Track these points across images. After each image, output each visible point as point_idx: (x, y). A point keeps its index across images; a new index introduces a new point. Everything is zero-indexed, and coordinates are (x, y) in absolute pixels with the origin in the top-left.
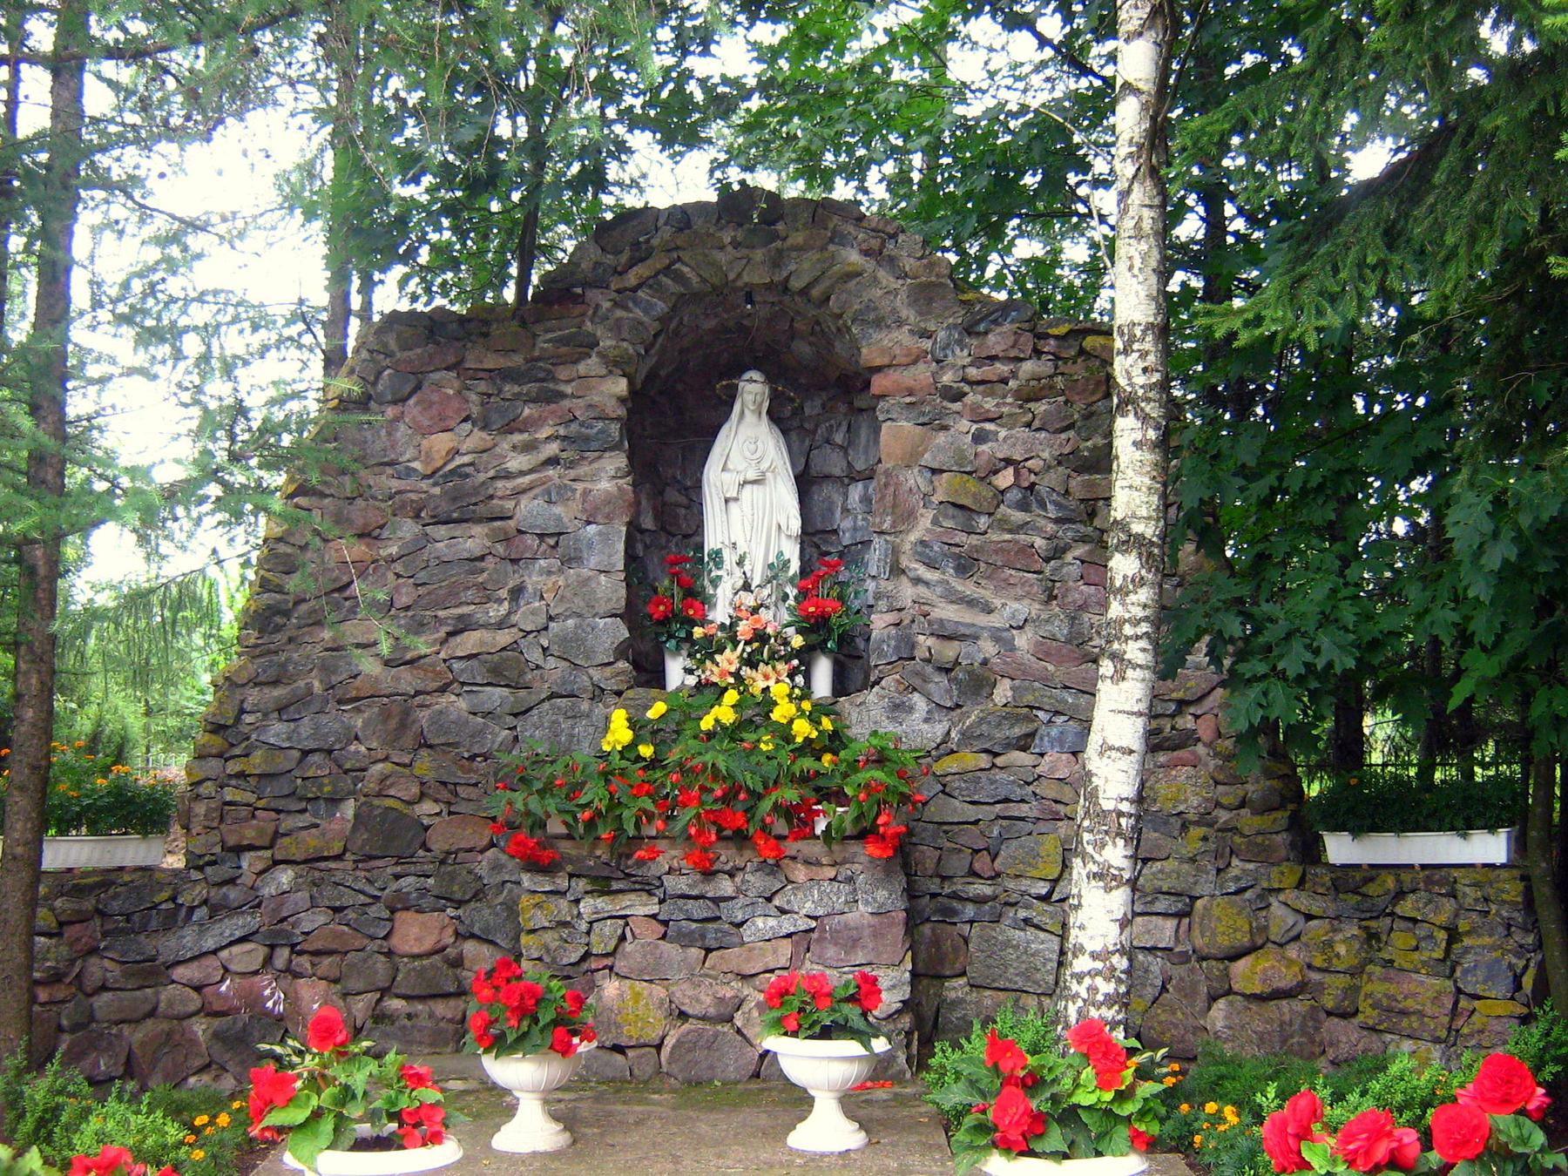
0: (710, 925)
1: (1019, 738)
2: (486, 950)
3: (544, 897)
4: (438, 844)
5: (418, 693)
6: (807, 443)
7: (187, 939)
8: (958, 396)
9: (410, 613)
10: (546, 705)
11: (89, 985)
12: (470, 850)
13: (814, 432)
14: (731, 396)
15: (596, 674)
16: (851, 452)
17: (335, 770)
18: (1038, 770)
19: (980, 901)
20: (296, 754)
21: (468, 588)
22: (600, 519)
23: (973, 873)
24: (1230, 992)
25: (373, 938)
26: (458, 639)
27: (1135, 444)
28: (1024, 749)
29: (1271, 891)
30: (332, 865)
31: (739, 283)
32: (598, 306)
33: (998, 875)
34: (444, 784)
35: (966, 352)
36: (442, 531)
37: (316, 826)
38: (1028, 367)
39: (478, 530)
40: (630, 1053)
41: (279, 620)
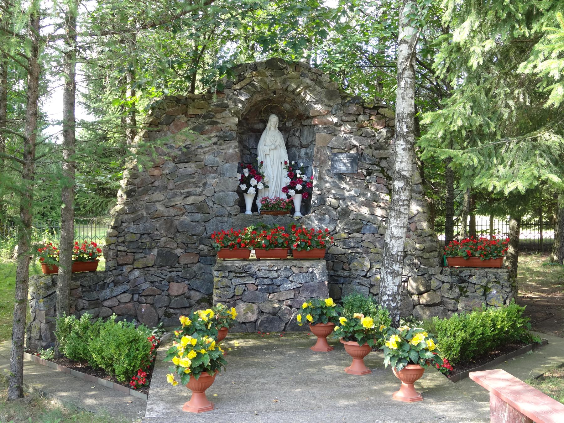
0: (270, 286)
2: (197, 293)
3: (221, 279)
4: (183, 261)
5: (175, 216)
6: (287, 135)
7: (107, 293)
9: (173, 191)
10: (214, 219)
11: (79, 308)
12: (192, 263)
14: (265, 122)
15: (228, 209)
17: (151, 240)
18: (362, 239)
19: (345, 277)
20: (139, 235)
21: (190, 183)
22: (230, 162)
23: (343, 269)
25: (163, 291)
26: (187, 199)
27: (403, 149)
28: (358, 232)
30: (151, 269)
31: (272, 88)
32: (228, 95)
33: (351, 270)
34: (184, 243)
35: (342, 112)
36: (181, 165)
37: (146, 257)
39: (193, 165)
40: (247, 325)
41: (133, 193)
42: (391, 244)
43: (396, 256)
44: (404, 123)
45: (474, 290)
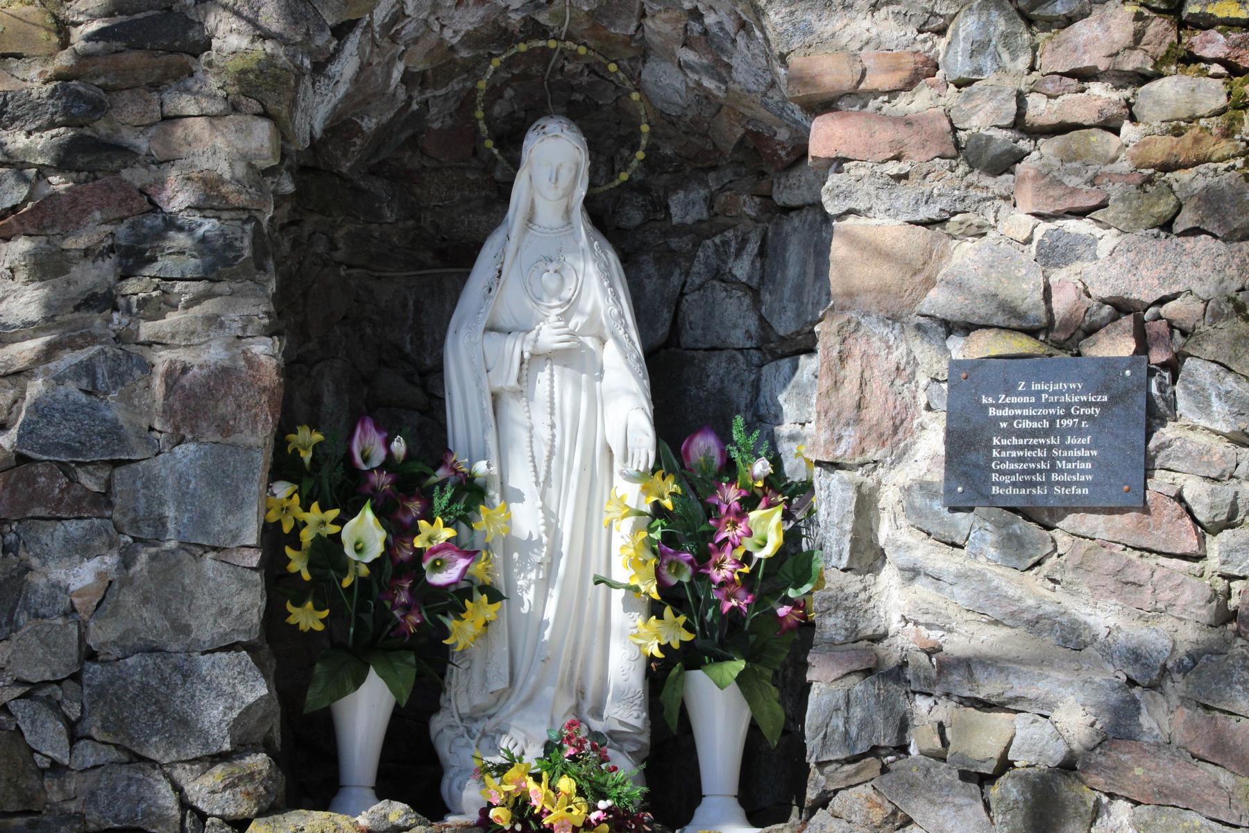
8: (1005, 163)
13: (691, 257)
16: (766, 297)
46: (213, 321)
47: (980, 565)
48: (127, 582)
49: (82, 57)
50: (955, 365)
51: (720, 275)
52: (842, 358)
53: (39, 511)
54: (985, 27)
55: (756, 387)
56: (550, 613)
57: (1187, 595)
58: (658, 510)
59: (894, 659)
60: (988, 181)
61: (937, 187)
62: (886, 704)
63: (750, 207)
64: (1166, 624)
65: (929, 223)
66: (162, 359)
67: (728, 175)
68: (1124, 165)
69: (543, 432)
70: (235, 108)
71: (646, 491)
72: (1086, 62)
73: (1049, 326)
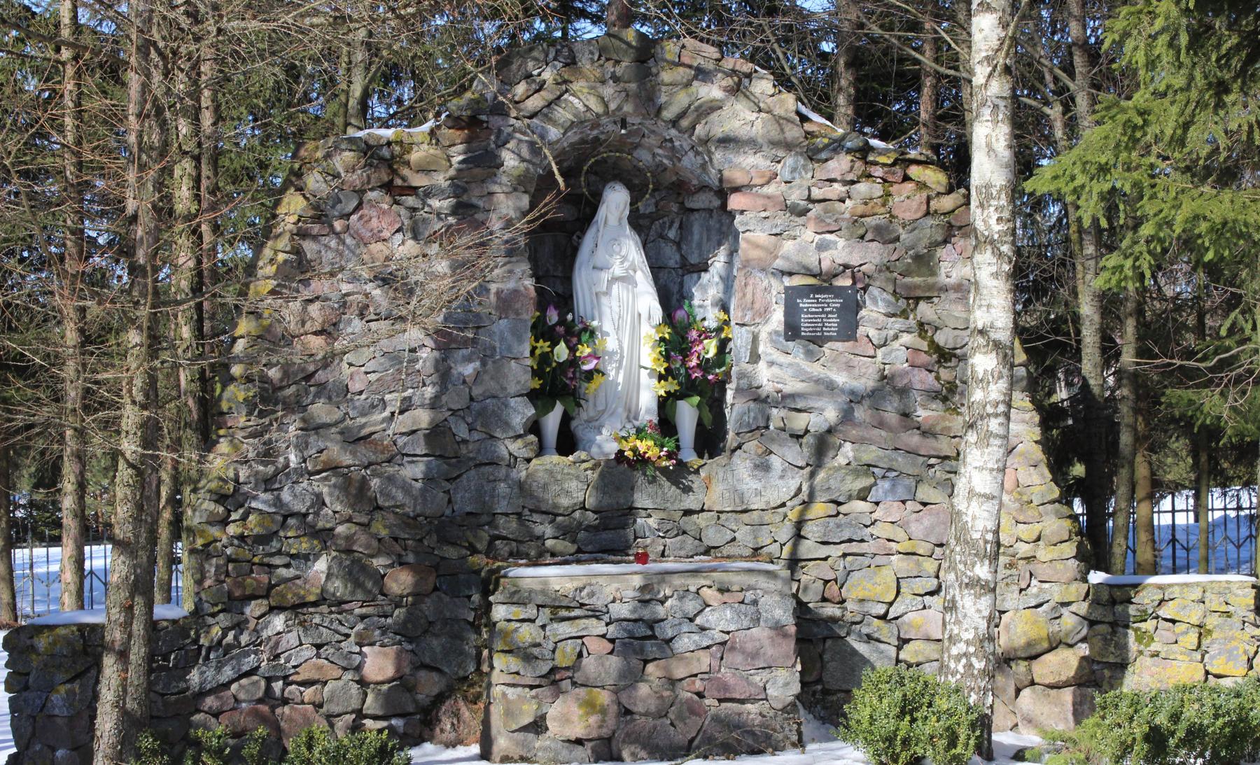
1: (860, 490)
8: (804, 212)
10: (473, 472)
13: (650, 228)
18: (874, 516)
20: (280, 518)
24: (1033, 683)
29: (1065, 604)
30: (311, 610)
38: (863, 188)
42: (970, 513)
43: (981, 542)
44: (992, 209)
45: (1171, 637)
46: (510, 272)
47: (797, 360)
48: (485, 372)
49: (459, 170)
50: (787, 288)
51: (662, 236)
52: (746, 285)
53: (454, 346)
54: (796, 162)
55: (681, 284)
56: (620, 379)
57: (871, 370)
58: (662, 339)
59: (764, 396)
60: (797, 219)
61: (779, 222)
62: (762, 412)
63: (675, 208)
64: (863, 380)
65: (776, 235)
66: (493, 287)
67: (664, 193)
68: (847, 215)
69: (616, 309)
70: (515, 190)
71: (658, 332)
72: (833, 176)
73: (820, 274)
